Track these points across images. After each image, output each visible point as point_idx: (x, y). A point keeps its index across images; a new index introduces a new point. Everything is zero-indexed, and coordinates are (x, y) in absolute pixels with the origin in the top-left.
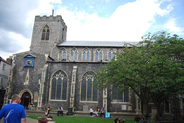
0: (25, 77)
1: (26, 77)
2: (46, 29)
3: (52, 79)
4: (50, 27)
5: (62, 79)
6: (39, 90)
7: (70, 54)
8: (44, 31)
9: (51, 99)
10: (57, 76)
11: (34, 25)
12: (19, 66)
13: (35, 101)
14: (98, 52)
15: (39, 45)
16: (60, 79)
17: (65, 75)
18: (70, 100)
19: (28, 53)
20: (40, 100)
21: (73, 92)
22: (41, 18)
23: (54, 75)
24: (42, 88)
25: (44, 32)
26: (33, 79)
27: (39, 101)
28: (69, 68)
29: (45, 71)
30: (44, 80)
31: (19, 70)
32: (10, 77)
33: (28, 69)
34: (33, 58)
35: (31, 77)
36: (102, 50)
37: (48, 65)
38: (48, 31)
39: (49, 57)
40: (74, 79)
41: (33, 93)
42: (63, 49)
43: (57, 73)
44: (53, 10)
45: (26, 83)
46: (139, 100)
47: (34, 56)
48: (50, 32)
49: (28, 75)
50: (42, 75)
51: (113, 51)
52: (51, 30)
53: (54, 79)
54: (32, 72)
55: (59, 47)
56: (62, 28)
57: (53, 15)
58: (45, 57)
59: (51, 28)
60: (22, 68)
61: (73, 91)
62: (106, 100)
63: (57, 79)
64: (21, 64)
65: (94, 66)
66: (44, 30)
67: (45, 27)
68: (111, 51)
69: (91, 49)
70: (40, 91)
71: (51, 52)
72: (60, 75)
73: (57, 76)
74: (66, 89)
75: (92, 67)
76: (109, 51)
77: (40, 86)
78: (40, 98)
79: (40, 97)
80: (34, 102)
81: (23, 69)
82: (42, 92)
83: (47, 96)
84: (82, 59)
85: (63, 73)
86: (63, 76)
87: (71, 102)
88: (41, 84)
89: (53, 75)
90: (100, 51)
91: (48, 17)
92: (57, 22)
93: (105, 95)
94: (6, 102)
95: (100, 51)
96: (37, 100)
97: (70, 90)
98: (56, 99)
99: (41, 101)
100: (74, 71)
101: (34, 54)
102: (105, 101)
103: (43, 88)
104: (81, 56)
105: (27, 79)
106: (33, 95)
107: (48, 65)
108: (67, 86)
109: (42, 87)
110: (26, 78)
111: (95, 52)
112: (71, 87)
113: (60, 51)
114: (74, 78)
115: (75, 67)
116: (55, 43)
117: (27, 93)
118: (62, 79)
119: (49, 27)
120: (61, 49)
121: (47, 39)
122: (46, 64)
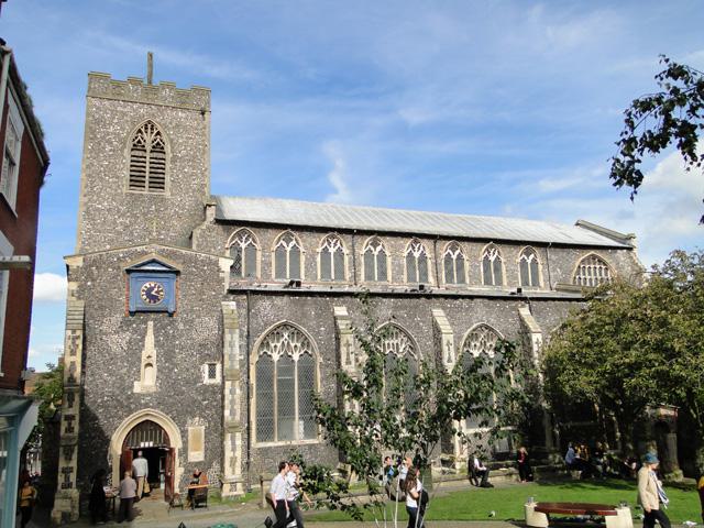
0: (139, 359)
1: (144, 358)
2: (149, 138)
5: (296, 357)
7: (273, 255)
9: (259, 439)
10: (275, 346)
12: (101, 308)
14: (285, 244)
15: (123, 209)
16: (287, 358)
20: (234, 450)
22: (118, 85)
23: (465, 345)
25: (137, 153)
26: (176, 365)
28: (318, 316)
31: (104, 328)
33: (151, 323)
35: (167, 354)
38: (158, 148)
41: (182, 426)
45: (147, 382)
48: (169, 156)
49: (150, 348)
51: (339, 245)
52: (172, 148)
53: (265, 359)
54: (166, 335)
58: (219, 270)
59: (171, 141)
60: (118, 318)
63: (276, 357)
64: (111, 299)
65: (401, 308)
66: (139, 142)
67: (140, 131)
69: (350, 236)
75: (396, 308)
78: (233, 444)
79: (233, 439)
89: (258, 341)
90: (291, 245)
94: (67, 478)
95: (291, 245)
98: (276, 439)
101: (171, 255)
103: (238, 401)
106: (184, 434)
111: (363, 252)
113: (233, 239)
117: (148, 428)
118: (296, 357)
119: (158, 133)
120: (239, 235)
121: (157, 183)
122: (225, 298)
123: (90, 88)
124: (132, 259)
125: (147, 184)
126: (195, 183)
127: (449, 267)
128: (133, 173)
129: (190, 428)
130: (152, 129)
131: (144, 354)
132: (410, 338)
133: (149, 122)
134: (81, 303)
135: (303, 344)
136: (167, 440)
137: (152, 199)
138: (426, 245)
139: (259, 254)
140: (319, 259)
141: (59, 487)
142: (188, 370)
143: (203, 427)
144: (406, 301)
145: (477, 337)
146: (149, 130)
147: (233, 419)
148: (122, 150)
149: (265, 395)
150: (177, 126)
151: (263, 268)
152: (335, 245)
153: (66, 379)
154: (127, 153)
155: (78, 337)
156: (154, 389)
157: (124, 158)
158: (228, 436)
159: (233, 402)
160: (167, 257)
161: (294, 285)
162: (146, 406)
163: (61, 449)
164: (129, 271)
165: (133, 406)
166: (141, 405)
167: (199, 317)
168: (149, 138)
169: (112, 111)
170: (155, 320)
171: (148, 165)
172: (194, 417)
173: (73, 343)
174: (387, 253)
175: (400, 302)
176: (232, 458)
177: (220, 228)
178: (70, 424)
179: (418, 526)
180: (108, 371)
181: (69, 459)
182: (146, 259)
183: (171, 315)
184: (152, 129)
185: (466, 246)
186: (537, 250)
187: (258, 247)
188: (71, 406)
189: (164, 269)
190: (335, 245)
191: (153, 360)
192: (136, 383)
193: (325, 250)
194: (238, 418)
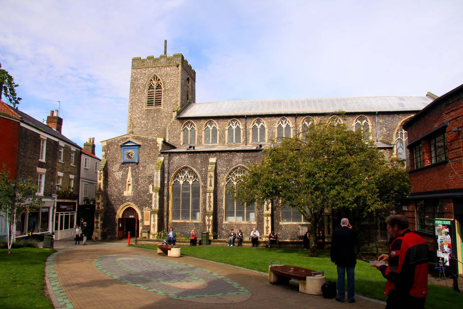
0: (126, 182)
2: (155, 82)
4: (163, 80)
6: (151, 203)
7: (203, 132)
8: (151, 87)
9: (173, 218)
10: (182, 177)
11: (132, 77)
12: (113, 161)
13: (146, 223)
15: (144, 116)
17: (195, 176)
18: (206, 220)
19: (127, 138)
20: (154, 221)
21: (210, 206)
22: (143, 61)
24: (155, 201)
25: (151, 90)
26: (139, 185)
27: (152, 223)
29: (160, 170)
30: (155, 205)
31: (114, 169)
32: (100, 183)
33: (130, 168)
34: (137, 147)
35: (136, 180)
36: (264, 122)
37: (163, 158)
38: (159, 87)
39: (164, 142)
40: (211, 181)
41: (141, 209)
42: (189, 122)
43: (181, 171)
44: (166, 41)
45: (128, 192)
46: (329, 218)
47: (139, 143)
48: (163, 89)
49: (129, 178)
50: (155, 176)
51: (231, 124)
52: (164, 85)
54: (136, 172)
55: (181, 120)
56: (186, 78)
57: (165, 53)
58: (157, 144)
59: (164, 83)
60: (118, 166)
61: (210, 204)
62: (269, 218)
63: (181, 182)
66: (151, 85)
67: (151, 80)
68: (282, 122)
69: (244, 119)
70: (153, 205)
71: (167, 131)
72: (186, 176)
73: (182, 177)
74: (198, 200)
75: (244, 158)
76: (279, 123)
77: (153, 197)
78: (154, 219)
79: (154, 217)
80: (145, 226)
81: (121, 168)
82: (157, 208)
83: (165, 214)
84: (226, 142)
85: (191, 172)
86: (191, 177)
87: (207, 223)
88: (154, 194)
90: (260, 125)
91: (157, 60)
92: (176, 68)
93: (268, 210)
94: (97, 225)
95: (260, 125)
96: (149, 222)
97: (204, 203)
99: (156, 223)
100: (211, 168)
101: (138, 138)
102: (268, 221)
104: (225, 136)
105: (129, 185)
106: (142, 213)
107: (163, 158)
108: (199, 196)
109: (156, 197)
110: (128, 183)
111: (251, 127)
112: (206, 197)
114: (211, 181)
115: (213, 160)
116: (174, 111)
117: (130, 210)
119: (159, 80)
120: (187, 124)
121: (159, 103)
122: (159, 156)
123: (132, 65)
124: (122, 141)
125: (154, 104)
128: (149, 100)
129: (144, 211)
130: (157, 78)
131: (128, 180)
135: (194, 177)
136: (138, 216)
137: (155, 110)
138: (290, 122)
139: (196, 132)
140: (227, 132)
141: (95, 228)
142: (144, 187)
143: (150, 212)
144: (250, 154)
145: (184, 172)
146: (155, 79)
147: (156, 208)
148: (144, 91)
149: (177, 199)
150: (166, 74)
152: (236, 124)
153: (98, 189)
154: (146, 92)
155: (101, 173)
156: (130, 195)
157: (145, 94)
160: (135, 139)
161: (192, 149)
162: (128, 201)
163: (95, 215)
164: (121, 146)
165: (124, 201)
166: (126, 200)
167: (148, 164)
169: (140, 73)
170: (131, 166)
172: (146, 207)
173: (100, 175)
174: (266, 127)
175: (246, 154)
176: (153, 225)
177: (178, 122)
178: (98, 206)
180: (115, 187)
181: (97, 219)
182: (128, 140)
183: (137, 164)
184: (157, 78)
186: (215, 121)
187: (196, 129)
188: (98, 199)
189: (134, 144)
190: (236, 124)
191: (131, 183)
193: (280, 127)
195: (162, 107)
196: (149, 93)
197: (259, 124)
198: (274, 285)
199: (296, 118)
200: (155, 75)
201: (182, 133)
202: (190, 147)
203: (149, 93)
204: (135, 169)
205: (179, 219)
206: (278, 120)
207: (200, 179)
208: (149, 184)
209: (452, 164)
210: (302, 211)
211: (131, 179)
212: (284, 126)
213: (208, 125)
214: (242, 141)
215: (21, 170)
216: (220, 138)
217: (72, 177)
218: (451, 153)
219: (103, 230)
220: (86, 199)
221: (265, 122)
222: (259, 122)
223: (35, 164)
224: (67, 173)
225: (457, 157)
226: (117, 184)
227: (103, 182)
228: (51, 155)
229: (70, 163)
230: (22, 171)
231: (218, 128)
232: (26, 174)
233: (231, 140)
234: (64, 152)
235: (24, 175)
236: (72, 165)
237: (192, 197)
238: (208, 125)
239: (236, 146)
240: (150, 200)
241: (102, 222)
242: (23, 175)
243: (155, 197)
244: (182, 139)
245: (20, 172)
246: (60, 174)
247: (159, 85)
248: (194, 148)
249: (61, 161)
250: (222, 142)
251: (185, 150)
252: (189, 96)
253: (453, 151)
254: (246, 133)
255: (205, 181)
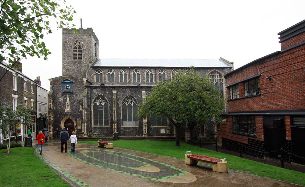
1: (67, 104)
2: (77, 45)
3: (92, 104)
5: (103, 104)
6: (82, 116)
7: (107, 76)
8: (75, 48)
10: (98, 101)
11: (63, 40)
12: (57, 91)
16: (100, 104)
17: (106, 101)
20: (84, 127)
21: (115, 118)
31: (58, 96)
33: (68, 95)
35: (72, 103)
37: (87, 90)
38: (80, 47)
40: (114, 104)
41: (76, 120)
43: (98, 98)
44: (81, 20)
45: (68, 110)
48: (82, 49)
49: (68, 101)
51: (122, 72)
52: (83, 47)
53: (95, 105)
54: (71, 98)
58: (83, 81)
59: (82, 45)
60: (60, 94)
61: (114, 116)
62: (146, 124)
63: (98, 104)
66: (75, 46)
67: (75, 43)
68: (148, 72)
70: (83, 118)
77: (83, 112)
78: (84, 125)
81: (62, 96)
85: (103, 98)
86: (103, 102)
87: (114, 127)
90: (137, 72)
91: (78, 30)
95: (112, 73)
101: (72, 78)
103: (86, 115)
104: (119, 78)
106: (76, 122)
107: (87, 90)
109: (84, 113)
111: (132, 74)
115: (115, 92)
118: (103, 104)
119: (80, 43)
121: (80, 57)
122: (85, 89)
125: (78, 58)
126: (89, 57)
127: (160, 76)
132: (135, 100)
133: (77, 40)
134: (53, 90)
136: (74, 124)
139: (103, 76)
150: (84, 40)
151: (104, 80)
154: (72, 49)
155: (51, 98)
156: (69, 111)
158: (83, 123)
159: (84, 115)
161: (103, 85)
168: (77, 45)
170: (69, 94)
171: (78, 52)
174: (140, 74)
179: (303, 111)
181: (50, 126)
182: (66, 79)
184: (78, 42)
185: (166, 70)
190: (124, 72)
191: (69, 104)
192: (65, 110)
193: (147, 74)
194: (86, 119)
195: (82, 60)
196: (74, 51)
197: (111, 72)
198: (191, 166)
199: (155, 69)
200: (77, 40)
201: (95, 75)
202: (102, 84)
203: (74, 51)
204: (71, 96)
205: (97, 125)
206: (107, 70)
207: (108, 103)
208: (80, 105)
209: (263, 97)
210: (89, 113)
211: (69, 102)
212: (149, 74)
213: (109, 72)
214: (128, 81)
215: (3, 96)
216: (116, 79)
217: (32, 100)
218: (263, 91)
219: (54, 133)
220: (41, 114)
221: (139, 72)
222: (136, 71)
223: (11, 92)
224: (30, 98)
225: (265, 94)
226: (61, 105)
227: (52, 103)
228: (20, 86)
229: (31, 92)
230: (3, 97)
231: (115, 74)
232: (6, 98)
233: (148, 81)
234: (27, 85)
235: (5, 99)
236: (32, 93)
237: (104, 112)
238: (109, 72)
239: (125, 84)
240: (81, 114)
241: (52, 128)
242: (4, 100)
243: (84, 113)
244: (95, 79)
245: (2, 97)
246: (26, 99)
247: (80, 46)
248: (104, 84)
249: (26, 90)
250: (117, 82)
251: (99, 86)
252: (95, 55)
253: (264, 90)
254: (130, 77)
255: (111, 103)
